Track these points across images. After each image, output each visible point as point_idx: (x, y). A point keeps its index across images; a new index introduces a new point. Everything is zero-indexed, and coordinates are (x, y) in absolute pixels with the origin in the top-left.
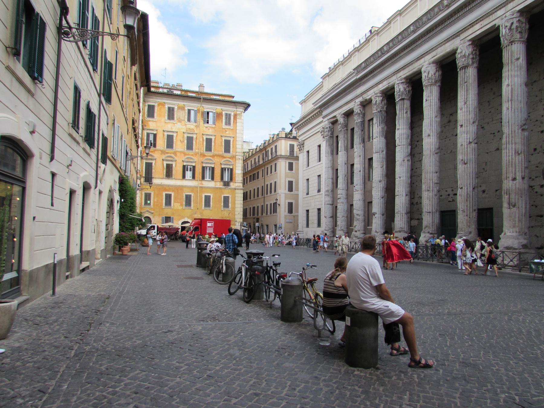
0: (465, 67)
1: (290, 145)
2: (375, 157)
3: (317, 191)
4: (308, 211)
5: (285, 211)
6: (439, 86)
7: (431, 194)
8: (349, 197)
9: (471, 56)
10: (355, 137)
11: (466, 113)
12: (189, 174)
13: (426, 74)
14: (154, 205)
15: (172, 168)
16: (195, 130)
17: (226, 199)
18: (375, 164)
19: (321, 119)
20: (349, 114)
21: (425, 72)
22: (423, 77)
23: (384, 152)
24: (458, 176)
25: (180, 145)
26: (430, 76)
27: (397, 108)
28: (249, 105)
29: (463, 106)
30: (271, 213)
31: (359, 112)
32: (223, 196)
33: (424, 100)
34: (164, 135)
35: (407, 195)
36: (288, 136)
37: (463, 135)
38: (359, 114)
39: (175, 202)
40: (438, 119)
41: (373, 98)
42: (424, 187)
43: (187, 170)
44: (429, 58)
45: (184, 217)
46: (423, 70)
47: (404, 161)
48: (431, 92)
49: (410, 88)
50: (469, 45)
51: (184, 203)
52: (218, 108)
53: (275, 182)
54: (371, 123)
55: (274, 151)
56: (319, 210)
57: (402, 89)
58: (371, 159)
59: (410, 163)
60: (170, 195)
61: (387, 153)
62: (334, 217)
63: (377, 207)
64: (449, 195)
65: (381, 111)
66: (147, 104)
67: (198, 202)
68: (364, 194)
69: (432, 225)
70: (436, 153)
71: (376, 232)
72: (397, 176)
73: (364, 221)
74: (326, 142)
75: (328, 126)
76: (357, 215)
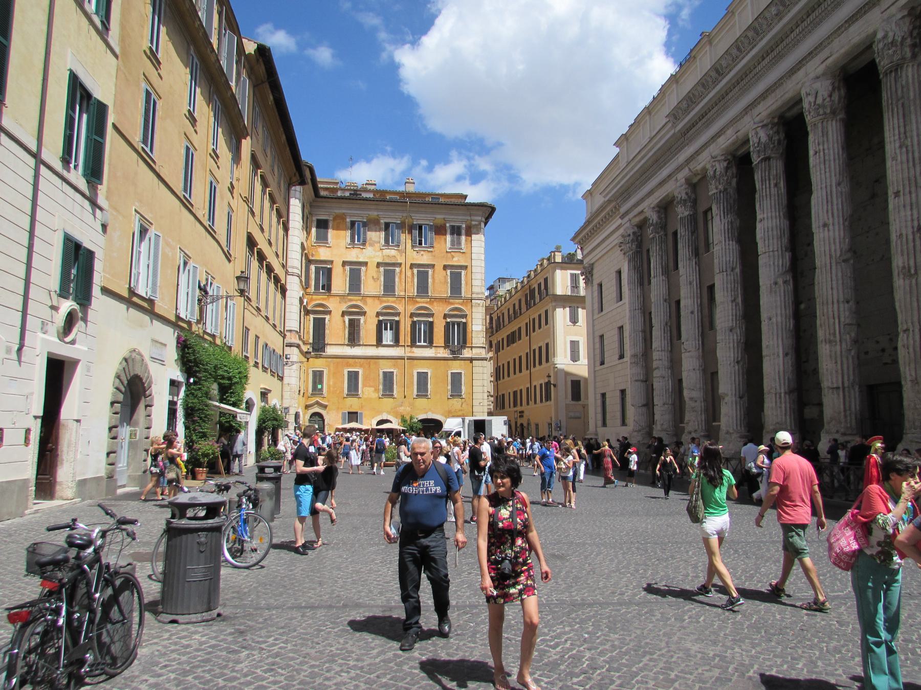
0: (897, 68)
1: (572, 275)
2: (719, 281)
3: (617, 357)
4: (603, 395)
5: (566, 397)
6: (840, 120)
7: (838, 347)
8: (675, 364)
9: (909, 41)
10: (680, 246)
11: (905, 166)
12: (388, 336)
13: (811, 99)
14: (328, 391)
15: (359, 326)
16: (398, 257)
17: (456, 379)
18: (719, 296)
19: (620, 221)
20: (665, 207)
21: (808, 94)
22: (806, 105)
23: (738, 270)
24: (897, 305)
25: (372, 284)
26: (819, 101)
27: (757, 177)
28: (492, 210)
29: (898, 151)
30: (541, 401)
31: (684, 196)
32: (450, 372)
33: (811, 153)
34: (344, 270)
35: (787, 354)
36: (570, 261)
37: (902, 214)
38: (685, 201)
39: (364, 386)
40: (845, 188)
41: (708, 166)
42: (821, 334)
43: (386, 329)
44: (816, 67)
45: (380, 413)
46: (803, 92)
47: (776, 283)
48: (825, 133)
49: (782, 136)
50: (903, 17)
51: (381, 387)
52: (438, 216)
53: (547, 345)
54: (709, 217)
55: (543, 287)
56: (623, 392)
57: (764, 139)
58: (711, 288)
59: (791, 287)
60: (357, 373)
61: (743, 272)
62: (649, 405)
63: (728, 383)
64: (883, 350)
65: (725, 189)
66: (314, 219)
67: (405, 385)
68: (703, 356)
69: (845, 416)
70: (844, 261)
71: (727, 433)
72: (764, 315)
73: (706, 410)
74: (629, 261)
75: (630, 231)
76: (691, 399)
